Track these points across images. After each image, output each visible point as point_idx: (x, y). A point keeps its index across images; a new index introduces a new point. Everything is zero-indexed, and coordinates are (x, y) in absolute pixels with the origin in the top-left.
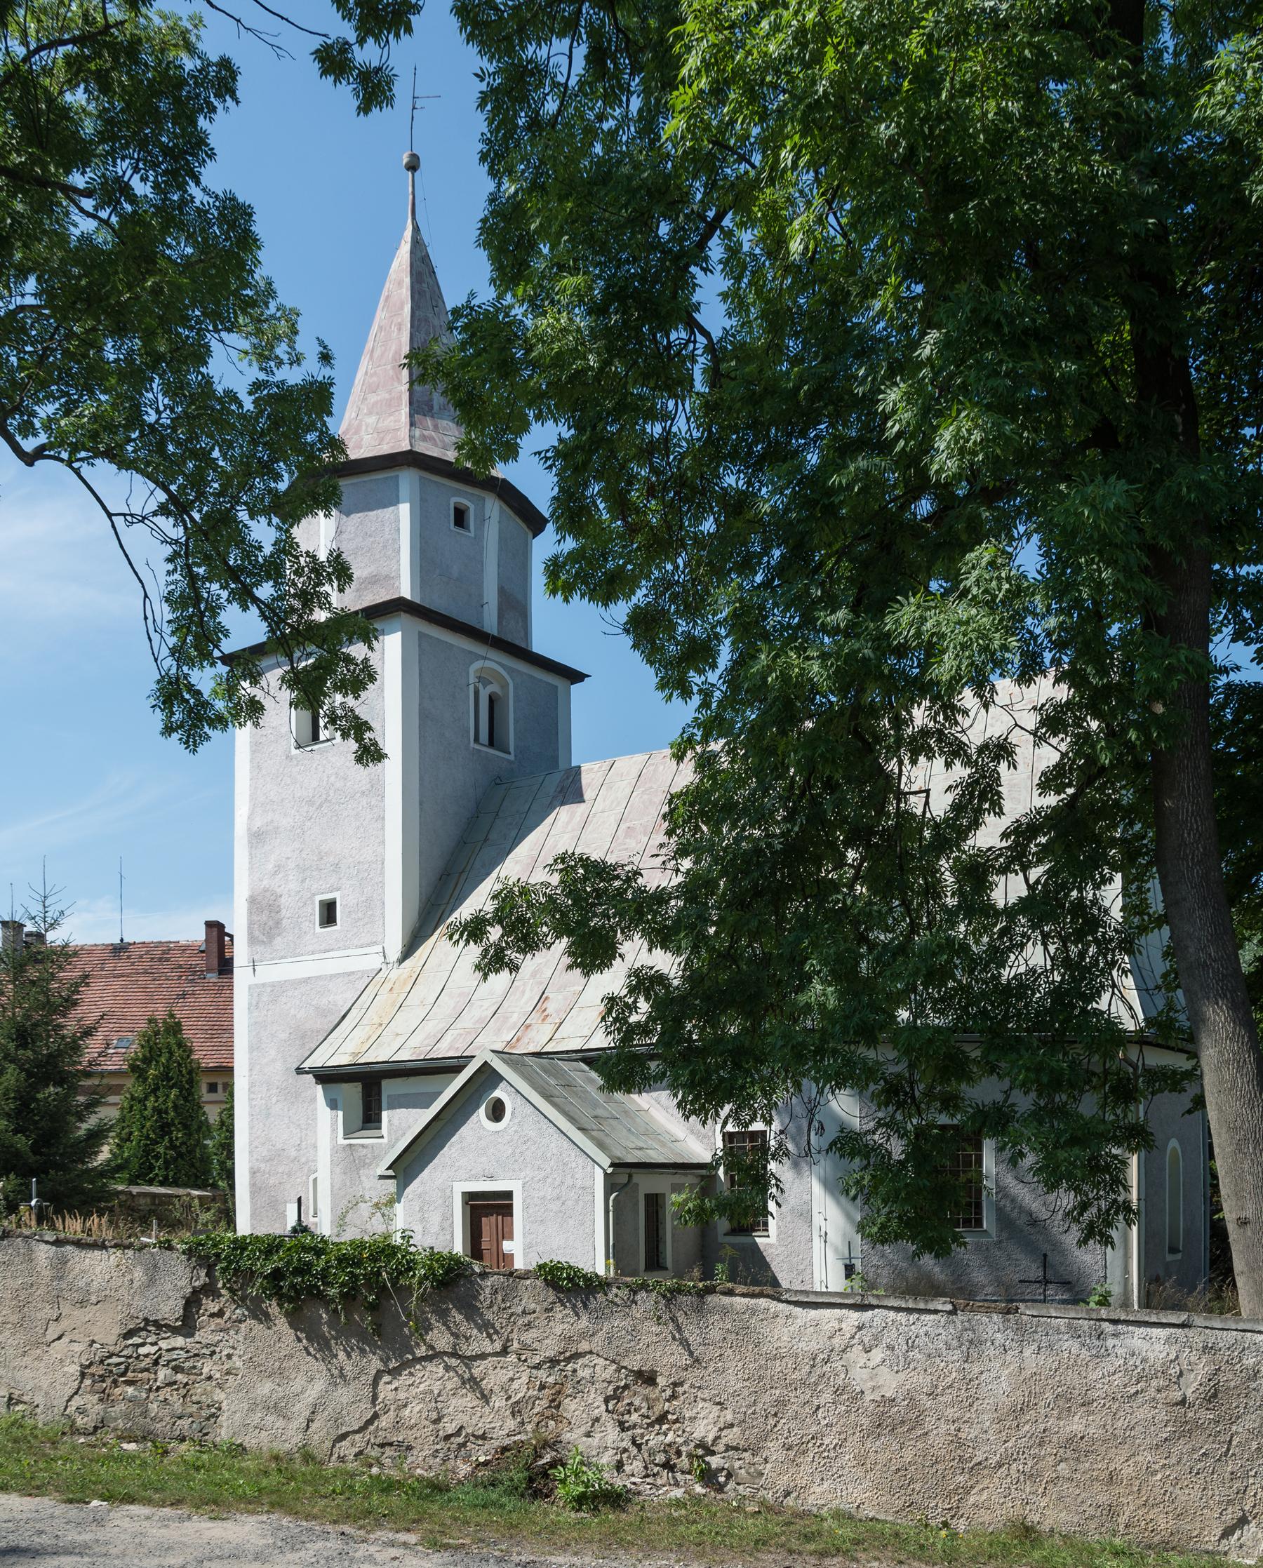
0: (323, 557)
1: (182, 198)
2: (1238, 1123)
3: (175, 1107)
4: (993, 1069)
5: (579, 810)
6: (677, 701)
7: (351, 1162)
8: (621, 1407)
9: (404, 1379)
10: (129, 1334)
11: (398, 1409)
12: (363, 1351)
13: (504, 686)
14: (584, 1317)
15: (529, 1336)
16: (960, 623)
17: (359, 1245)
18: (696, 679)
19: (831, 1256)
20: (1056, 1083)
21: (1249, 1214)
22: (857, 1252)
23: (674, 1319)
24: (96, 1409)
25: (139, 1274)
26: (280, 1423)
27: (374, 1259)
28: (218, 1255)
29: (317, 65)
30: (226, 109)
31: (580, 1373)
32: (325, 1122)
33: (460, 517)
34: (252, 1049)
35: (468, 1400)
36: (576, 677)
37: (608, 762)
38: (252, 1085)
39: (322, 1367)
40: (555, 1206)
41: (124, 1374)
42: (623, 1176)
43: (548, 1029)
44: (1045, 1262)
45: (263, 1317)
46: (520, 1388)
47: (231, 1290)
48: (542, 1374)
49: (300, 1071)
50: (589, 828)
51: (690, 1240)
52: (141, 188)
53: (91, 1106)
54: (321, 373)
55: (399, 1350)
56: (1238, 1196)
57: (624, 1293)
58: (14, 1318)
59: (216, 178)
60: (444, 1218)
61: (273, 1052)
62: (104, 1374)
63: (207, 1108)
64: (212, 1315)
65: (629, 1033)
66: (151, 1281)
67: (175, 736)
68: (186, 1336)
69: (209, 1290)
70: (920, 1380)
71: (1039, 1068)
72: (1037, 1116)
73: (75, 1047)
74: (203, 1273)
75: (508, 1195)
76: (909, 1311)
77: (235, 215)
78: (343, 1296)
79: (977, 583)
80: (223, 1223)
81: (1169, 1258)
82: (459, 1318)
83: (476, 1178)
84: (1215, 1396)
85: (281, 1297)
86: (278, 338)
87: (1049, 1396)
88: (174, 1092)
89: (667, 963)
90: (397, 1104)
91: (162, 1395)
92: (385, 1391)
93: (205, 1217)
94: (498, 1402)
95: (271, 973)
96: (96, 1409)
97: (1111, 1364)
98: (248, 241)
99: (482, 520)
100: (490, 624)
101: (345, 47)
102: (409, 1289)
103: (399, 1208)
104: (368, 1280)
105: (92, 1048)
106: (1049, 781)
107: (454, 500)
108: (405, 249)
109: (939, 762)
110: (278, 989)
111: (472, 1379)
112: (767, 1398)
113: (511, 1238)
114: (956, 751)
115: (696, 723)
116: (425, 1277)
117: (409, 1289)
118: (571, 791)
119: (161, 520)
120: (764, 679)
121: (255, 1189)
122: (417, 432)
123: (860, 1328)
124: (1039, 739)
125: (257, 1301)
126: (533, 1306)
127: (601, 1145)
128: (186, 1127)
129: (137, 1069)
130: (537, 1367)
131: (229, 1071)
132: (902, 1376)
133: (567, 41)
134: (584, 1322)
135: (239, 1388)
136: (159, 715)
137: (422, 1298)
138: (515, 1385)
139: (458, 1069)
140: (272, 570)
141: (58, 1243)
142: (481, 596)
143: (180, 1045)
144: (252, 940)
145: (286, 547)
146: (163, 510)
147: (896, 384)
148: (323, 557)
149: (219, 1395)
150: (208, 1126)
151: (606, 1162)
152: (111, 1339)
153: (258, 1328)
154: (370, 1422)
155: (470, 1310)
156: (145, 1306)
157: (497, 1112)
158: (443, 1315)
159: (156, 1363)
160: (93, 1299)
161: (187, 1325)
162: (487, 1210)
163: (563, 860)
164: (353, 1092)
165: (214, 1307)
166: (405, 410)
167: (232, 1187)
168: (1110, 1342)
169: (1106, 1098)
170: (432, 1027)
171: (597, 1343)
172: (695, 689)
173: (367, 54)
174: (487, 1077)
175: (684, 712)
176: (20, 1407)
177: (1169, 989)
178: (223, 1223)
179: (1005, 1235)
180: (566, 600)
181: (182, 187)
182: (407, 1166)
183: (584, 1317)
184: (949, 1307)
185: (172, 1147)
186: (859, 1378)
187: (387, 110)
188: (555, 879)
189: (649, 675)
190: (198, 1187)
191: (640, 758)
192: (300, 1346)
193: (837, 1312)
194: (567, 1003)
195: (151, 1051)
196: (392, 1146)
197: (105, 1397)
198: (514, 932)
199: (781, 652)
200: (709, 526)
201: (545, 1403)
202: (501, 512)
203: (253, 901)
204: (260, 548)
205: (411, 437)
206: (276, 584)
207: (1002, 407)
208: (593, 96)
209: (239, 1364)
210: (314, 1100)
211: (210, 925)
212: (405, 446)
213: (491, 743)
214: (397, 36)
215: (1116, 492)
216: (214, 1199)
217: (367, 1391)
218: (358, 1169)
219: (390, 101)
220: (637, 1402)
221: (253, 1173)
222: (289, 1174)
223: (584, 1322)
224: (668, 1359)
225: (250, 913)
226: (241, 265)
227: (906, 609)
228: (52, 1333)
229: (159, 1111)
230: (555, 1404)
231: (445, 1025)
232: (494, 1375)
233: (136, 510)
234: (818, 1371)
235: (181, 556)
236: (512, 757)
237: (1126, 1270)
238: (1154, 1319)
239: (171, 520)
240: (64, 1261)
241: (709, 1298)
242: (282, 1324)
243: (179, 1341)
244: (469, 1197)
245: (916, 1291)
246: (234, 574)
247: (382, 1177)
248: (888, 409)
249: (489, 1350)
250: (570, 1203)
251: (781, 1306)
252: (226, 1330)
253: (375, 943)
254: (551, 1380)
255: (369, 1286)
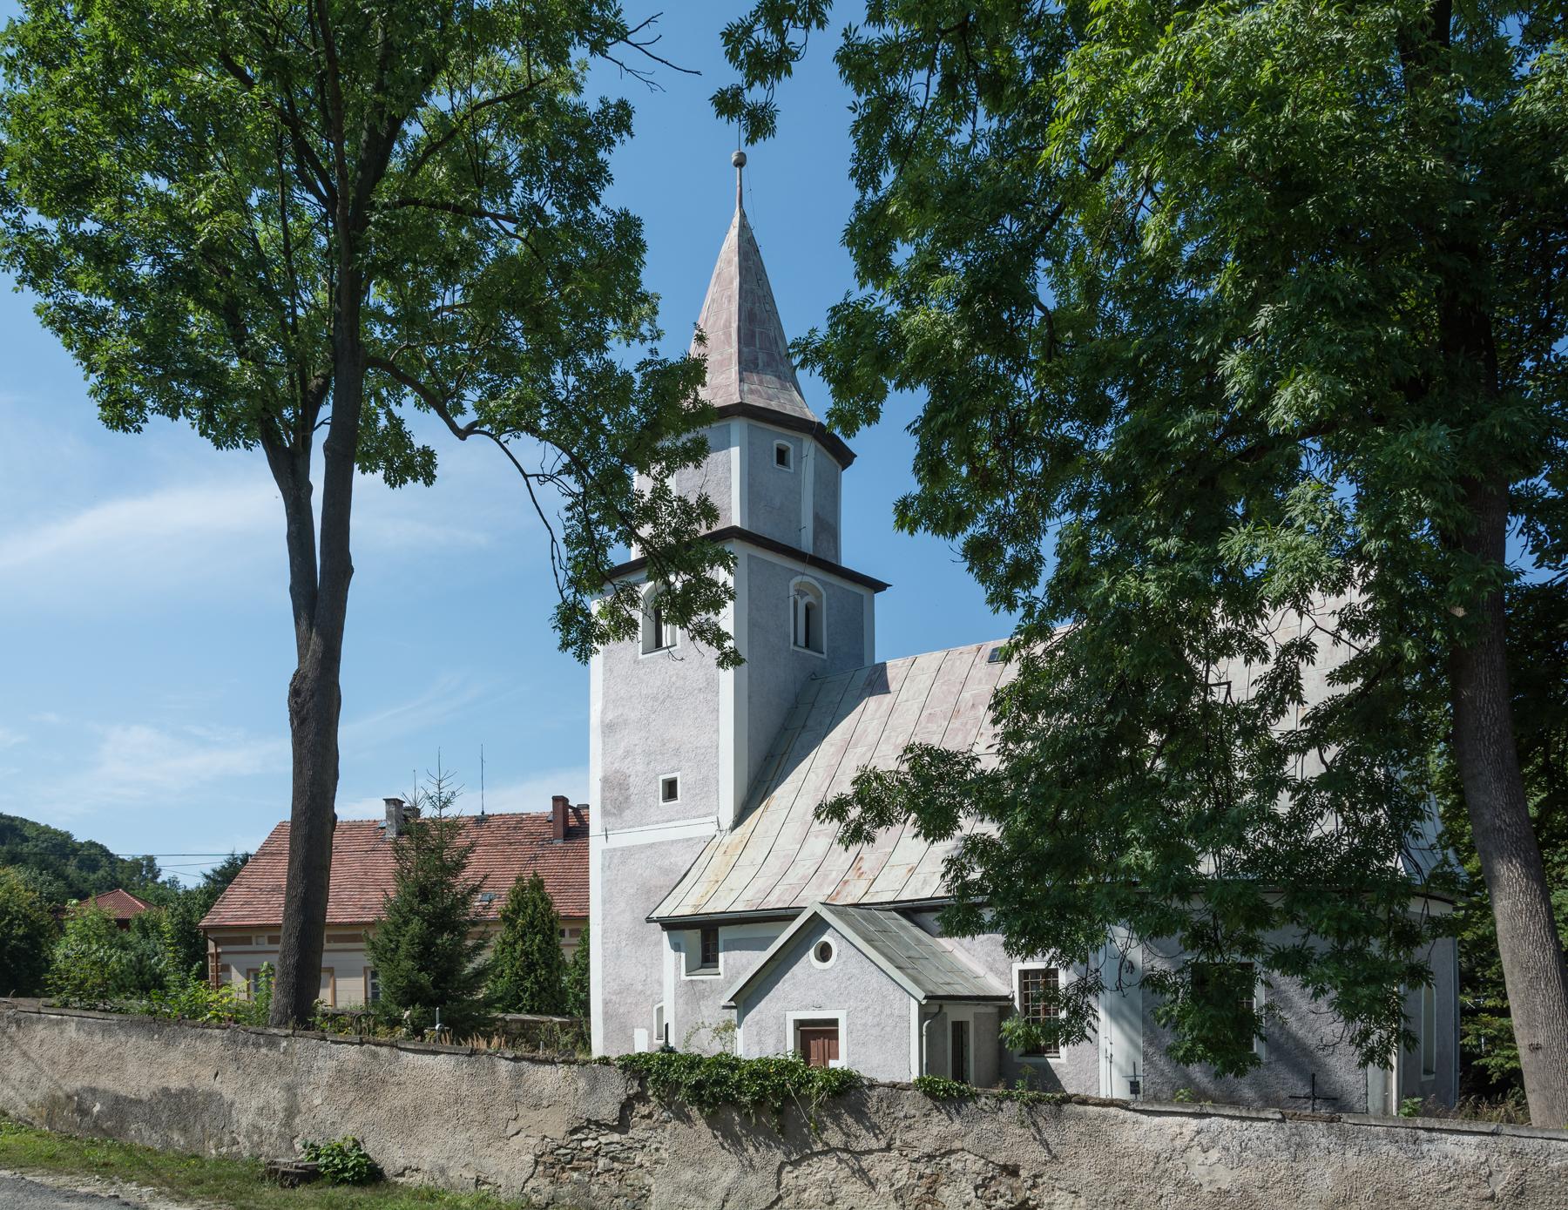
0: (692, 500)
1: (585, 216)
2: (1531, 964)
3: (539, 949)
4: (1294, 918)
5: (886, 699)
6: (1003, 612)
7: (693, 996)
8: (988, 1193)
9: (803, 1169)
10: (574, 1131)
11: (799, 1193)
12: (768, 1146)
13: (818, 597)
14: (957, 1121)
15: (909, 1136)
16: (1288, 550)
17: (766, 1062)
18: (1020, 594)
19: (1115, 1073)
20: (1356, 929)
21: (1541, 1039)
22: (1140, 1072)
23: (1035, 1124)
24: (548, 1190)
25: (582, 1084)
26: (700, 1203)
27: (779, 1074)
28: (649, 1070)
29: (714, 108)
30: (623, 142)
31: (954, 1166)
32: (670, 963)
33: (782, 456)
34: (604, 902)
35: (859, 1186)
36: (879, 586)
37: (911, 659)
38: (604, 932)
39: (735, 1159)
40: (874, 1032)
41: (570, 1162)
42: (935, 1008)
43: (862, 885)
44: (1313, 1081)
45: (687, 1119)
46: (902, 1178)
47: (659, 1097)
48: (921, 1167)
49: (649, 920)
50: (895, 715)
51: (989, 1058)
52: (550, 209)
53: (478, 948)
54: (694, 350)
55: (800, 1150)
56: (1530, 1025)
57: (992, 1102)
58: (481, 1118)
59: (611, 199)
60: (779, 1041)
61: (623, 905)
62: (553, 1162)
63: (565, 951)
64: (643, 1117)
65: (965, 888)
66: (593, 1090)
67: (570, 650)
68: (621, 1133)
69: (641, 1097)
70: (1251, 1176)
71: (1341, 917)
72: (1337, 956)
73: (464, 901)
74: (636, 1084)
75: (835, 1022)
76: (1243, 1119)
77: (627, 226)
78: (754, 1102)
79: (1304, 512)
80: (580, 1045)
81: (1424, 1078)
82: (850, 1121)
83: (806, 1008)
84: (1522, 1193)
85: (700, 1102)
86: (641, 318)
87: (1369, 1190)
88: (539, 937)
89: (991, 829)
90: (732, 946)
91: (601, 1179)
92: (788, 1178)
93: (565, 1039)
94: (883, 1188)
95: (620, 840)
96: (548, 1190)
97: (1424, 1166)
98: (637, 247)
99: (800, 459)
100: (806, 544)
101: (737, 92)
102: (809, 1098)
103: (739, 1032)
104: (775, 1091)
105: (477, 902)
106: (1342, 675)
107: (777, 442)
108: (734, 233)
109: (1240, 659)
110: (627, 852)
111: (861, 1170)
112: (1116, 1189)
113: (837, 1058)
114: (1256, 650)
115: (1020, 630)
116: (823, 1088)
117: (809, 1098)
118: (877, 683)
119: (564, 478)
120: (1106, 599)
121: (607, 1017)
122: (746, 387)
123: (1198, 1133)
124: (1337, 638)
125: (682, 1105)
126: (913, 1112)
127: (916, 981)
128: (548, 965)
129: (508, 919)
130: (917, 1161)
131: (586, 919)
132: (1236, 1172)
133: (925, 72)
134: (957, 1125)
135: (666, 1174)
136: (559, 634)
137: (820, 1105)
138: (898, 1175)
139: (793, 918)
140: (649, 513)
141: (516, 1059)
142: (799, 522)
143: (543, 900)
144: (605, 813)
145: (661, 493)
146: (567, 470)
147: (1233, 351)
148: (692, 500)
149: (649, 1180)
150: (566, 965)
151: (921, 995)
152: (560, 1135)
153: (682, 1128)
154: (775, 1203)
155: (860, 1115)
156: (587, 1109)
157: (824, 953)
158: (837, 1119)
159: (596, 1154)
160: (545, 1103)
161: (622, 1125)
162: (817, 1034)
163: (911, 750)
164: (695, 936)
165: (645, 1110)
166: (735, 368)
167: (587, 1014)
168: (1425, 1147)
169: (1389, 941)
170: (762, 883)
171: (968, 1142)
172: (1020, 602)
173: (755, 95)
174: (817, 924)
175: (1011, 620)
176: (485, 1187)
177: (1443, 848)
178: (580, 1045)
179: (1273, 1058)
180: (911, 533)
181: (584, 207)
182: (747, 998)
183: (957, 1121)
184: (1279, 1116)
185: (537, 982)
186: (1198, 1173)
187: (770, 140)
188: (905, 767)
189: (980, 592)
190: (558, 1015)
191: (939, 655)
192: (716, 1142)
193: (1178, 1119)
194: (911, 864)
195: (519, 903)
196: (730, 983)
197: (555, 1180)
198: (865, 809)
199: (1120, 576)
200: (1037, 466)
201: (923, 1190)
202: (817, 450)
203: (605, 781)
204: (642, 496)
205: (741, 391)
206: (655, 525)
207: (1333, 366)
208: (943, 114)
209: (665, 1155)
210: (659, 943)
211: (556, 799)
212: (736, 399)
213: (807, 646)
214: (779, 78)
215: (1440, 436)
216: (571, 1025)
217: (773, 1179)
218: (698, 1001)
219: (772, 131)
220: (1002, 1190)
221: (606, 1003)
222: (636, 1005)
223: (957, 1125)
224: (1029, 1155)
225: (603, 790)
226: (631, 267)
227: (1236, 538)
228: (511, 1130)
229: (525, 953)
230: (932, 1191)
231: (772, 881)
232: (879, 1167)
233: (547, 472)
234: (1161, 1167)
235: (579, 502)
236: (825, 656)
237: (1386, 1088)
238: (1465, 1128)
239: (573, 477)
240: (520, 1074)
241: (1065, 1107)
242: (701, 1124)
243: (616, 1137)
244: (800, 1024)
245: (1197, 1101)
246: (624, 518)
247: (725, 1007)
248: (1227, 373)
249: (875, 1147)
250: (888, 1029)
251: (1129, 1114)
252: (655, 1129)
253: (711, 814)
254: (928, 1171)
255: (775, 1095)
